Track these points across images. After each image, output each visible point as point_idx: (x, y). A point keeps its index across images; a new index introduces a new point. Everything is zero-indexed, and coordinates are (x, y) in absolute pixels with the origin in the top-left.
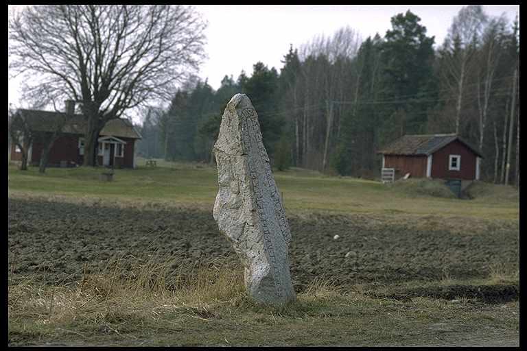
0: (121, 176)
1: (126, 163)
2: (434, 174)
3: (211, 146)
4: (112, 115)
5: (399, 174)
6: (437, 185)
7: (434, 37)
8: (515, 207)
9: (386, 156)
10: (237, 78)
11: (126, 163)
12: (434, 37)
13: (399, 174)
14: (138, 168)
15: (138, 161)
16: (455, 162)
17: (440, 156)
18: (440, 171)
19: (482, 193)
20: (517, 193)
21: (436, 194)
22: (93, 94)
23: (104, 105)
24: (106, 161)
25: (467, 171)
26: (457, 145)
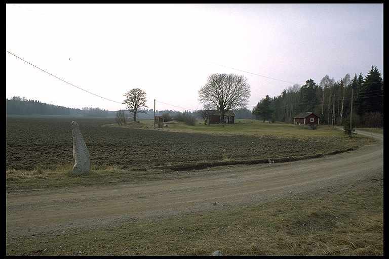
0: (229, 126)
1: (232, 122)
2: (306, 124)
3: (81, 111)
4: (227, 110)
5: (298, 123)
6: (308, 126)
7: (267, 96)
8: (381, 133)
9: (296, 118)
10: (255, 105)
11: (232, 122)
12: (267, 96)
13: (298, 123)
14: (236, 123)
15: (236, 121)
16: (312, 120)
17: (308, 118)
18: (308, 122)
19: (320, 128)
20: (8, 116)
21: (306, 129)
22: (222, 107)
23: (225, 109)
24: (227, 122)
25: (316, 122)
26: (313, 115)
